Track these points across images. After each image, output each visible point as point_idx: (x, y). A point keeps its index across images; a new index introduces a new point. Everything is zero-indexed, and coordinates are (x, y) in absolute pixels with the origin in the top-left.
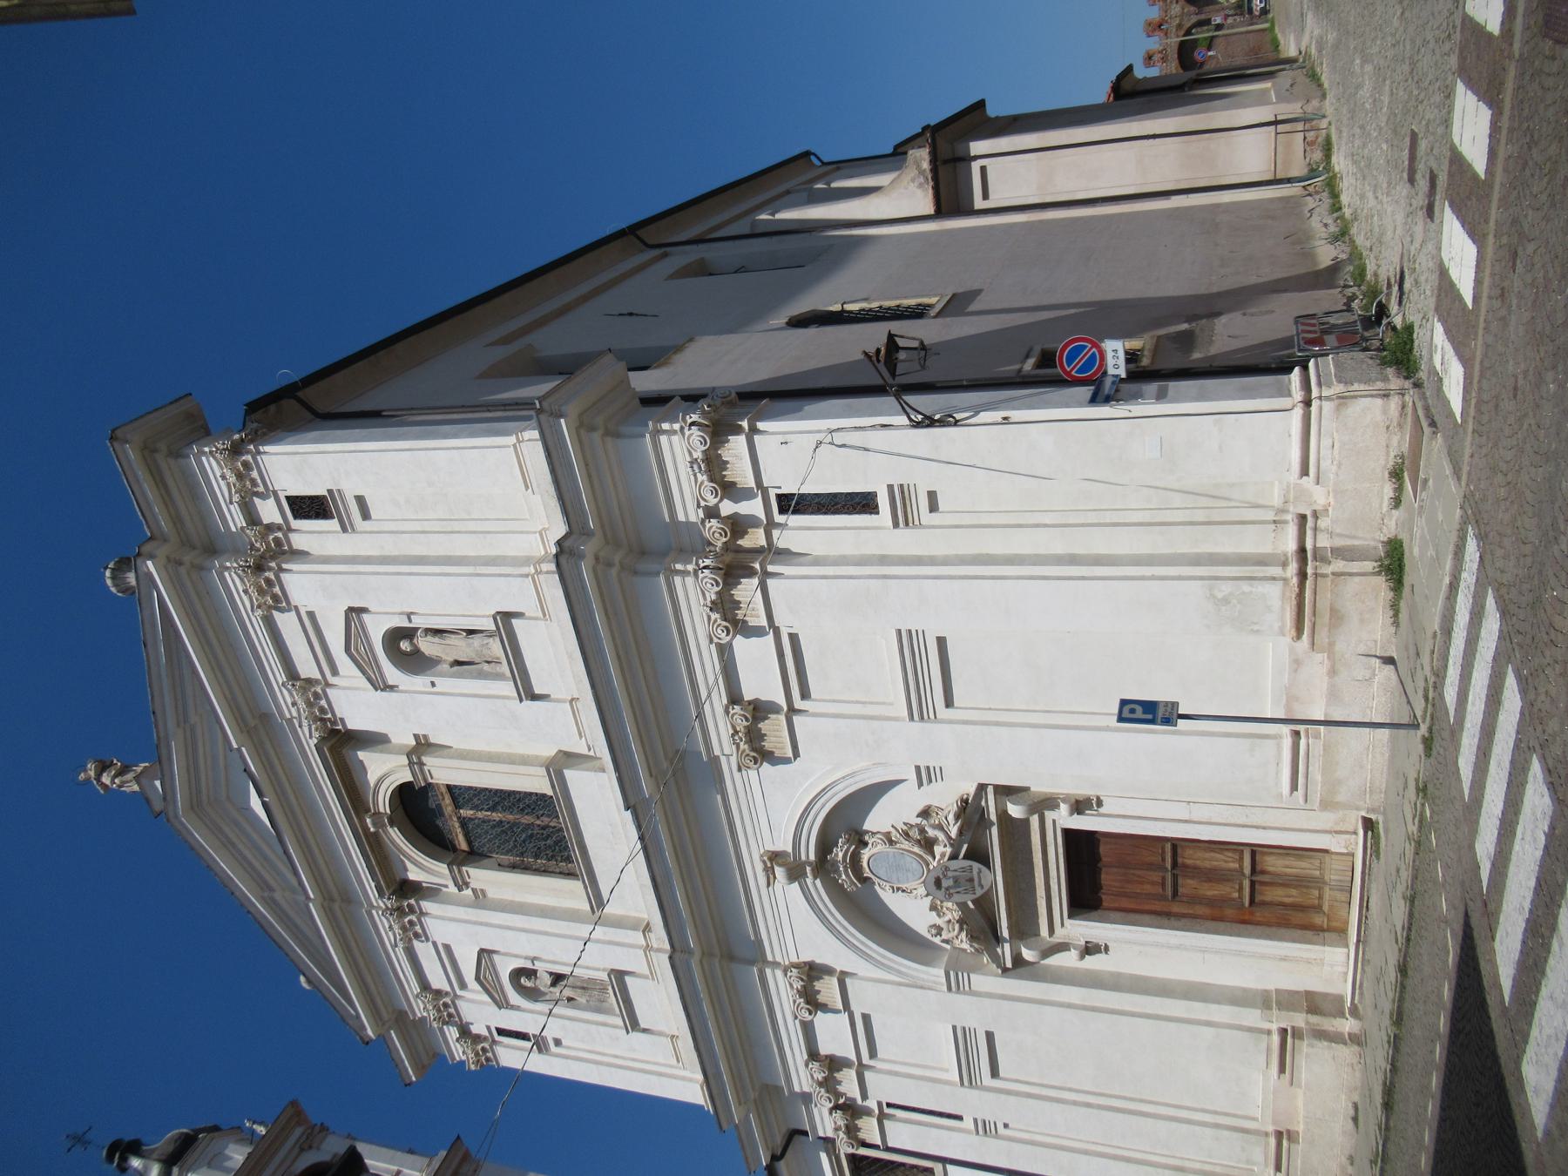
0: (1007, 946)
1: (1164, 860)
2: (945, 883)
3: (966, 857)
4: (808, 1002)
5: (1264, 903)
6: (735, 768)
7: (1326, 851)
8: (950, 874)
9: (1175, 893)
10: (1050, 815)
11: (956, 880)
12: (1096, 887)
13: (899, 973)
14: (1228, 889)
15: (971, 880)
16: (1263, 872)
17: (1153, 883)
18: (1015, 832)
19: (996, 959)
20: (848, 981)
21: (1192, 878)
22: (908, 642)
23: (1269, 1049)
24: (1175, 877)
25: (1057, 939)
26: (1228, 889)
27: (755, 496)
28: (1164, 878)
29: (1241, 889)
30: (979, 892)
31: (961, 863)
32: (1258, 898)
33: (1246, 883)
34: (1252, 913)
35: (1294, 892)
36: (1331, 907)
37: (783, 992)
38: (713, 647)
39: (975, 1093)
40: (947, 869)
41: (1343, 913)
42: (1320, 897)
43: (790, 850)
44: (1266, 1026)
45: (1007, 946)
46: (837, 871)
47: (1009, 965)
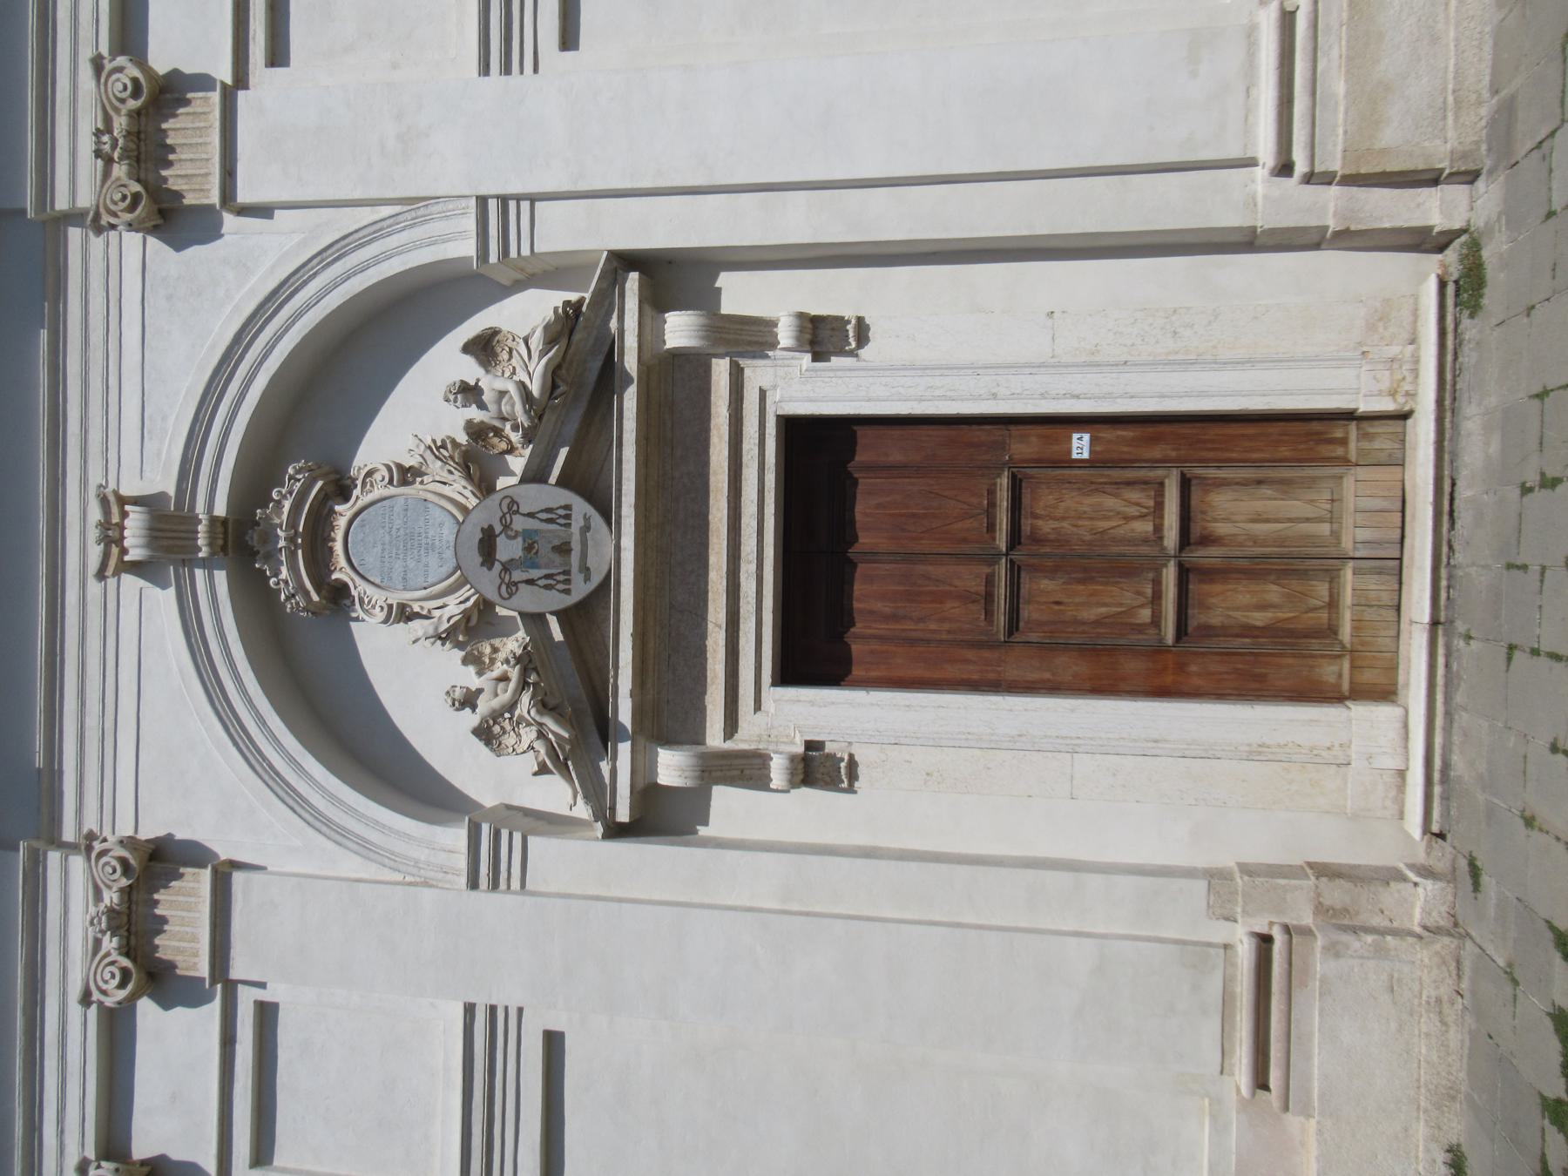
0: (624, 749)
1: (991, 528)
2: (508, 549)
3: (563, 482)
4: (127, 951)
5: (1208, 631)
6: (75, 991)
7: (1349, 416)
8: (519, 523)
9: (1013, 625)
10: (757, 374)
12: (842, 617)
13: (365, 848)
14: (1128, 598)
15: (564, 549)
16: (1207, 540)
17: (966, 597)
18: (677, 386)
19: (596, 792)
20: (238, 877)
21: (1052, 572)
22: (486, 1031)
23: (1227, 1000)
24: (1015, 570)
25: (741, 743)
26: (1128, 598)
27: (208, 999)
28: (990, 581)
29: (1157, 596)
30: (581, 589)
31: (551, 495)
32: (1196, 618)
33: (1170, 575)
34: (1181, 667)
35: (1273, 592)
36: (1358, 626)
37: (76, 900)
38: (93, 1011)
39: (529, 900)
40: (513, 506)
41: (1384, 642)
42: (1333, 604)
43: (172, 492)
44: (1219, 932)
45: (624, 749)
46: (271, 557)
47: (623, 815)
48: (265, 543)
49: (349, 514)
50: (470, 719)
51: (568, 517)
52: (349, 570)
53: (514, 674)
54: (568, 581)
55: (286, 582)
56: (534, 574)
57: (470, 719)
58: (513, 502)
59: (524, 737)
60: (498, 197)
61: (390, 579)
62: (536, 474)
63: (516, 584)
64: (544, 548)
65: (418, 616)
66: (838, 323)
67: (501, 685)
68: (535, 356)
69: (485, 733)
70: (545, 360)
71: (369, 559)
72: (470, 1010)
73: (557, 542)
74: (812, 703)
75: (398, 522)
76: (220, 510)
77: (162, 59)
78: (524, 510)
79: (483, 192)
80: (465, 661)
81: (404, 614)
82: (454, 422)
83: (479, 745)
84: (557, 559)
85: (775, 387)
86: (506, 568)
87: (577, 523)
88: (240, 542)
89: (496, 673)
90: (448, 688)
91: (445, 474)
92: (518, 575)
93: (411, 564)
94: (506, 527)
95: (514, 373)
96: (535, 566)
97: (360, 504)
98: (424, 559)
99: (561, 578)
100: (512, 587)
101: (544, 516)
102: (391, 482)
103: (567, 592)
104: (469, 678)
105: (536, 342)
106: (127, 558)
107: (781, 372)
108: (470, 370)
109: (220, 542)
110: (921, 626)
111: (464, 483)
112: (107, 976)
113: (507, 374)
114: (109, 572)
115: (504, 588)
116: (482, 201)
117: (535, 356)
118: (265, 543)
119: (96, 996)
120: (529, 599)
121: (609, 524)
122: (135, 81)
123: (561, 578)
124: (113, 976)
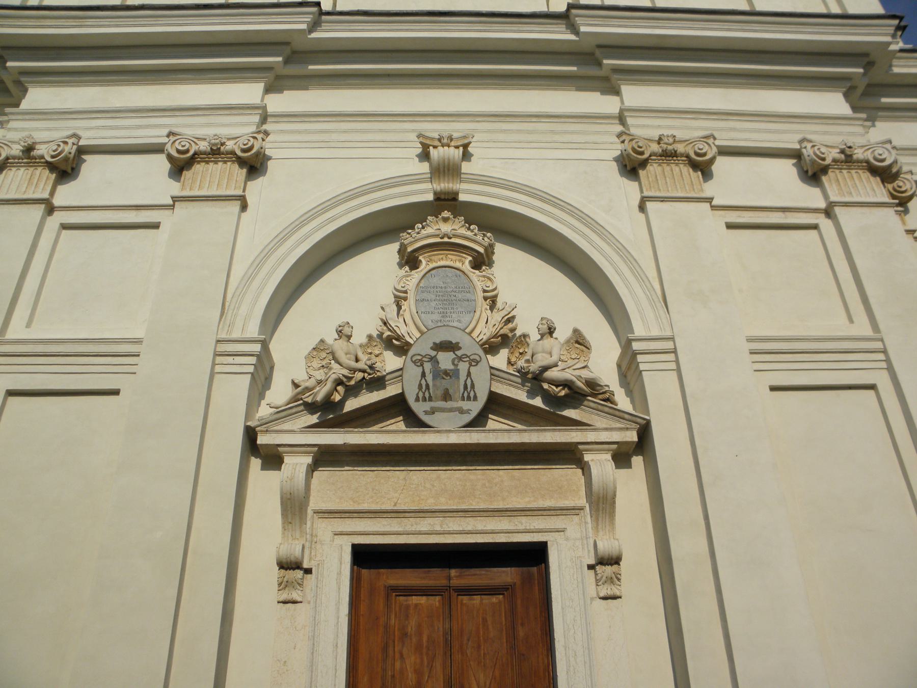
2: (445, 360)
11: (451, 374)
15: (446, 396)
22: (124, 352)
30: (419, 408)
48: (446, 221)
49: (463, 268)
50: (330, 337)
51: (469, 398)
53: (361, 365)
54: (424, 399)
55: (418, 233)
56: (429, 377)
57: (330, 337)
58: (477, 362)
59: (318, 372)
60: (675, 348)
61: (423, 292)
62: (494, 373)
63: (422, 365)
64: (446, 383)
65: (399, 308)
66: (615, 579)
67: (354, 358)
68: (577, 373)
69: (321, 347)
70: (574, 379)
71: (435, 280)
72: (138, 341)
73: (451, 391)
74: (339, 573)
75: (460, 296)
76: (462, 197)
77: (722, 165)
78: (473, 369)
79: (677, 340)
80: (370, 337)
81: (399, 300)
82: (527, 325)
83: (314, 343)
84: (440, 393)
85: (567, 539)
86: (433, 360)
87: (466, 405)
88: (447, 202)
90: (351, 324)
91: (493, 323)
92: (428, 366)
93: (433, 304)
94: (460, 358)
95: (562, 361)
96: (434, 378)
97: (471, 275)
99: (427, 395)
100: (420, 363)
102: (485, 291)
103: (417, 400)
104: (359, 338)
105: (585, 374)
106: (431, 148)
107: (578, 543)
108: (563, 333)
109: (443, 197)
110: (397, 655)
111: (488, 334)
112: (183, 144)
113: (562, 357)
114: (421, 139)
115: (419, 357)
116: (672, 339)
117: (577, 373)
118: (446, 221)
119: (172, 138)
120: (413, 372)
122: (704, 155)
123: (427, 395)
124: (183, 146)
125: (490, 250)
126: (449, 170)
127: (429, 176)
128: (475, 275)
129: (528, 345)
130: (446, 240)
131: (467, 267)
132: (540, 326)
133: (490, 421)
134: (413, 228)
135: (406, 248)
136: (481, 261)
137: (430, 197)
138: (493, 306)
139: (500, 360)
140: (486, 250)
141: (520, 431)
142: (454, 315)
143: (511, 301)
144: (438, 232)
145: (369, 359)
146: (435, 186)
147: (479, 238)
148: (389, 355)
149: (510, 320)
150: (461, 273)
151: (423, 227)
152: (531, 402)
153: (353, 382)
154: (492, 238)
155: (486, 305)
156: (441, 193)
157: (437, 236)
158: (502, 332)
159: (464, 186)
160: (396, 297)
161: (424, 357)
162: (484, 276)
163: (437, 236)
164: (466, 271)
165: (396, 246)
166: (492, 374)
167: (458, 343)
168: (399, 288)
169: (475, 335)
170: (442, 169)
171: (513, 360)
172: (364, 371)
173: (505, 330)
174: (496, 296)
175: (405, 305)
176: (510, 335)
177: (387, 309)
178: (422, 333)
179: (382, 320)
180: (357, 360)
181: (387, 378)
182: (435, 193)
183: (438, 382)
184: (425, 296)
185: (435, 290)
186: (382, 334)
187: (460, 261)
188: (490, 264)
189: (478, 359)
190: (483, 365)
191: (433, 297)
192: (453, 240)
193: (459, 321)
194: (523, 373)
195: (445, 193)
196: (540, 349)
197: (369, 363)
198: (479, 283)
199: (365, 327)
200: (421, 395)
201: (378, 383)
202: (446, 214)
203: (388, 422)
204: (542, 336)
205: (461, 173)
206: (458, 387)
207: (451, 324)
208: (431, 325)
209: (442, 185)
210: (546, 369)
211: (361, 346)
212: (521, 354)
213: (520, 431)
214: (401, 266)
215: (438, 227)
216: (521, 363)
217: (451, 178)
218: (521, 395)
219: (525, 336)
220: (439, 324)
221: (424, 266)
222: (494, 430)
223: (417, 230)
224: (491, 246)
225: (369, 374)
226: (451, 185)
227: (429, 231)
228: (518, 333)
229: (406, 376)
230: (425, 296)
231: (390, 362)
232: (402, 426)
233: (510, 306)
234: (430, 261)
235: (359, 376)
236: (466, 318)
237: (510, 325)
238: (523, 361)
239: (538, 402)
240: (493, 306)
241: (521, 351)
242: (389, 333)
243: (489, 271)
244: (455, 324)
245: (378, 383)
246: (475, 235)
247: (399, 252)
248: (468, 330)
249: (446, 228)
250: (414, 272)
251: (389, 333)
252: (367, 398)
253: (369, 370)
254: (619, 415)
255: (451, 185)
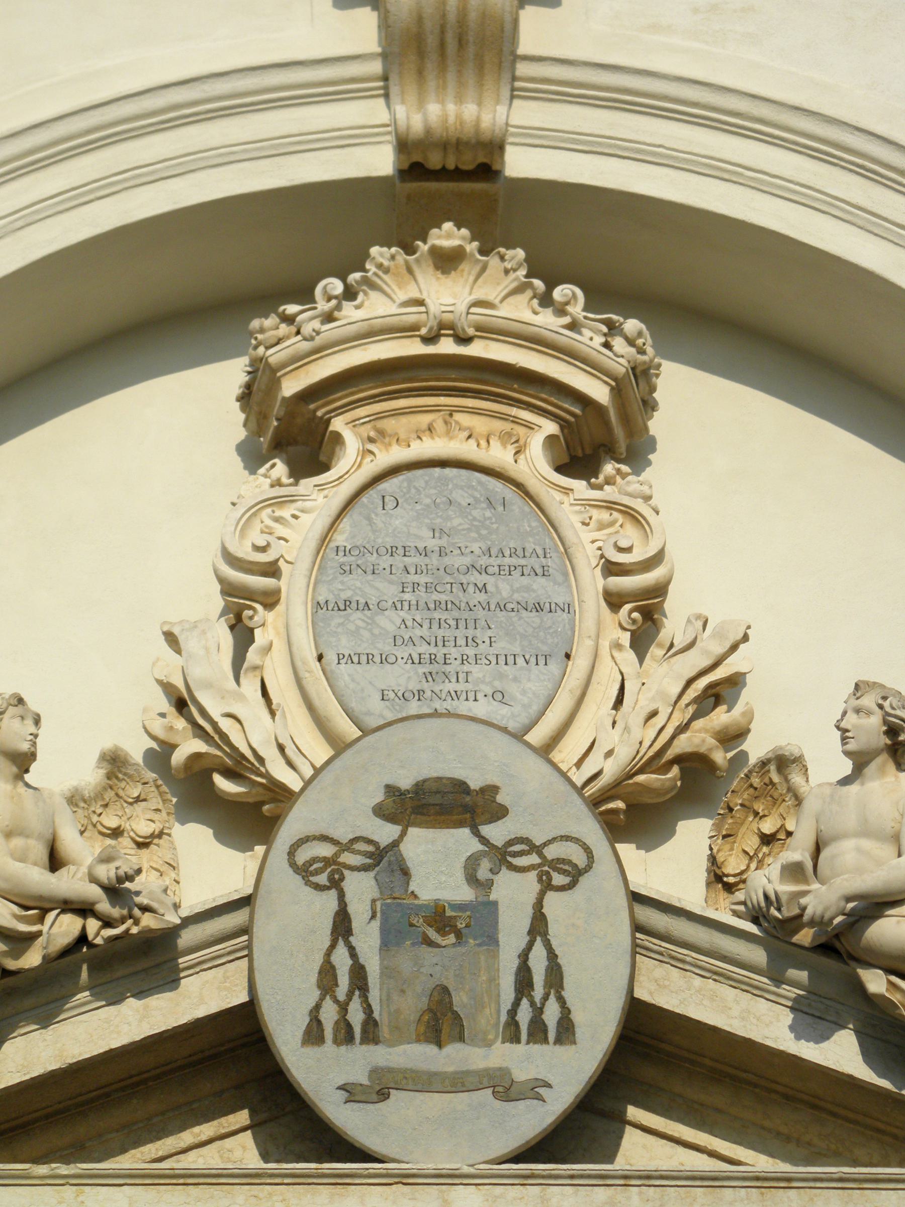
2: (437, 862)
15: (441, 1021)
30: (319, 1073)
49: (521, 470)
51: (538, 1032)
52: (370, 468)
53: (71, 883)
54: (345, 1035)
55: (329, 318)
56: (367, 937)
58: (576, 874)
61: (346, 570)
62: (650, 922)
63: (336, 883)
64: (437, 963)
65: (243, 635)
67: (40, 852)
71: (399, 520)
73: (460, 1000)
75: (503, 588)
76: (519, 163)
78: (554, 904)
80: (115, 762)
81: (243, 606)
82: (794, 712)
84: (412, 1005)
86: (385, 860)
87: (523, 1061)
88: (449, 183)
89: (72, 841)
90: (33, 704)
92: (361, 890)
93: (389, 622)
94: (502, 856)
96: (390, 939)
97: (551, 498)
98: (402, 652)
99: (356, 1016)
101: (538, 962)
102: (611, 569)
103: (313, 1034)
109: (434, 161)
111: (624, 756)
115: (326, 850)
120: (296, 920)
121: (518, 1157)
123: (356, 1016)
125: (636, 390)
126: (461, 42)
127: (376, 67)
128: (570, 501)
129: (799, 801)
130: (447, 347)
131: (535, 463)
132: (851, 720)
133: (631, 1137)
134: (305, 295)
135: (275, 383)
136: (598, 441)
137: (381, 161)
138: (644, 634)
139: (675, 866)
140: (618, 391)
141: (761, 1180)
142: (477, 671)
143: (725, 612)
144: (412, 315)
145: (106, 859)
146: (401, 111)
147: (590, 340)
148: (194, 840)
149: (718, 694)
150: (508, 492)
151: (350, 294)
152: (809, 1051)
153: (32, 959)
154: (647, 341)
155: (615, 629)
156: (429, 141)
157: (408, 330)
158: (683, 744)
159: (526, 114)
160: (229, 589)
161: (348, 846)
162: (610, 505)
163: (408, 330)
164: (533, 485)
165: (232, 373)
166: (638, 927)
167: (494, 789)
168: (245, 551)
169: (567, 754)
170: (432, 41)
171: (733, 865)
172: (84, 910)
173: (699, 738)
174: (660, 590)
175: (268, 627)
176: (720, 757)
177: (189, 642)
178: (339, 746)
179: (167, 688)
180: (55, 862)
181: (186, 938)
182: (403, 145)
183: (406, 958)
184: (356, 586)
185: (399, 561)
186: (169, 747)
187: (505, 438)
188: (637, 453)
189: (579, 859)
190: (601, 883)
191: (391, 592)
192: (477, 349)
193: (499, 696)
194: (775, 927)
195: (445, 145)
196: (849, 820)
197: (106, 872)
198: (586, 535)
199: (94, 714)
200: (329, 1014)
201: (142, 958)
202: (448, 236)
203: (187, 1137)
204: (861, 762)
205: (516, 58)
206: (493, 980)
207: (463, 707)
208: (377, 711)
209: (434, 109)
210: (875, 905)
211: (74, 799)
212: (767, 840)
213: (761, 1180)
214: (253, 457)
215: (412, 292)
216: (767, 880)
217: (471, 79)
218: (764, 1020)
219: (783, 762)
220: (414, 707)
221: (352, 462)
222: (647, 1178)
223: (323, 306)
224: (643, 374)
225: (108, 923)
226: (470, 110)
227: (374, 307)
228: (756, 748)
229: (266, 931)
230: (356, 586)
231: (200, 869)
232: (244, 1151)
233: (719, 634)
234: (380, 437)
235: (63, 929)
236: (530, 684)
237: (721, 717)
238: (774, 869)
239: (841, 1053)
240: (644, 634)
241: (768, 827)
242: (199, 746)
243: (633, 483)
244: (481, 709)
245: (142, 958)
246: (573, 326)
247: (246, 397)
248: (536, 736)
249: (447, 296)
250: (306, 484)
251: (199, 746)
252: (95, 1029)
253: (104, 906)
254: (353, 952)
255: (470, 110)
